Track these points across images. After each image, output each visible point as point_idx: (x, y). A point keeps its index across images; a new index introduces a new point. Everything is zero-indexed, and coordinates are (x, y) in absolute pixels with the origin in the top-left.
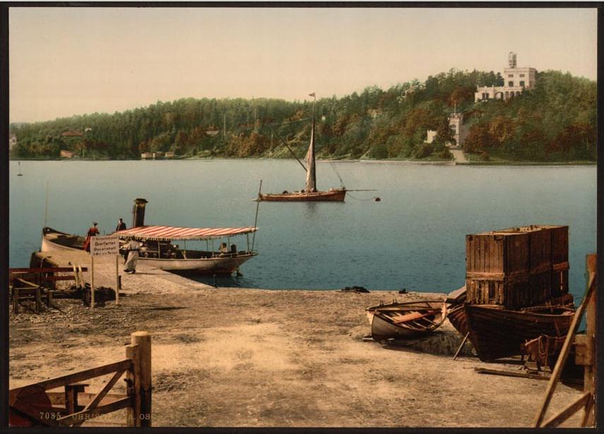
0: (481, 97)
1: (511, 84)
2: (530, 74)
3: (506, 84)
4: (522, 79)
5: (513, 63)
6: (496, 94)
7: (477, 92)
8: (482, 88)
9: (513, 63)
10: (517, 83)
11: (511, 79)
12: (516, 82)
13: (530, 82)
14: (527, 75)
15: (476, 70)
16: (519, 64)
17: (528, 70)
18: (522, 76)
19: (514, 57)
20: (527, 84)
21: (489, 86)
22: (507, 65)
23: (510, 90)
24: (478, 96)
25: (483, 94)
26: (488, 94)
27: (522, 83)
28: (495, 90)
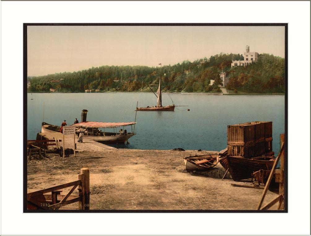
1: (247, 59)
3: (245, 59)
4: (252, 57)
5: (248, 50)
6: (240, 64)
7: (232, 63)
9: (248, 50)
10: (249, 59)
11: (247, 57)
12: (249, 59)
13: (256, 59)
14: (254, 55)
16: (251, 51)
17: (254, 53)
18: (252, 56)
19: (249, 47)
20: (254, 59)
22: (245, 51)
23: (246, 62)
24: (233, 65)
25: (235, 64)
26: (237, 64)
27: (252, 59)
28: (240, 62)
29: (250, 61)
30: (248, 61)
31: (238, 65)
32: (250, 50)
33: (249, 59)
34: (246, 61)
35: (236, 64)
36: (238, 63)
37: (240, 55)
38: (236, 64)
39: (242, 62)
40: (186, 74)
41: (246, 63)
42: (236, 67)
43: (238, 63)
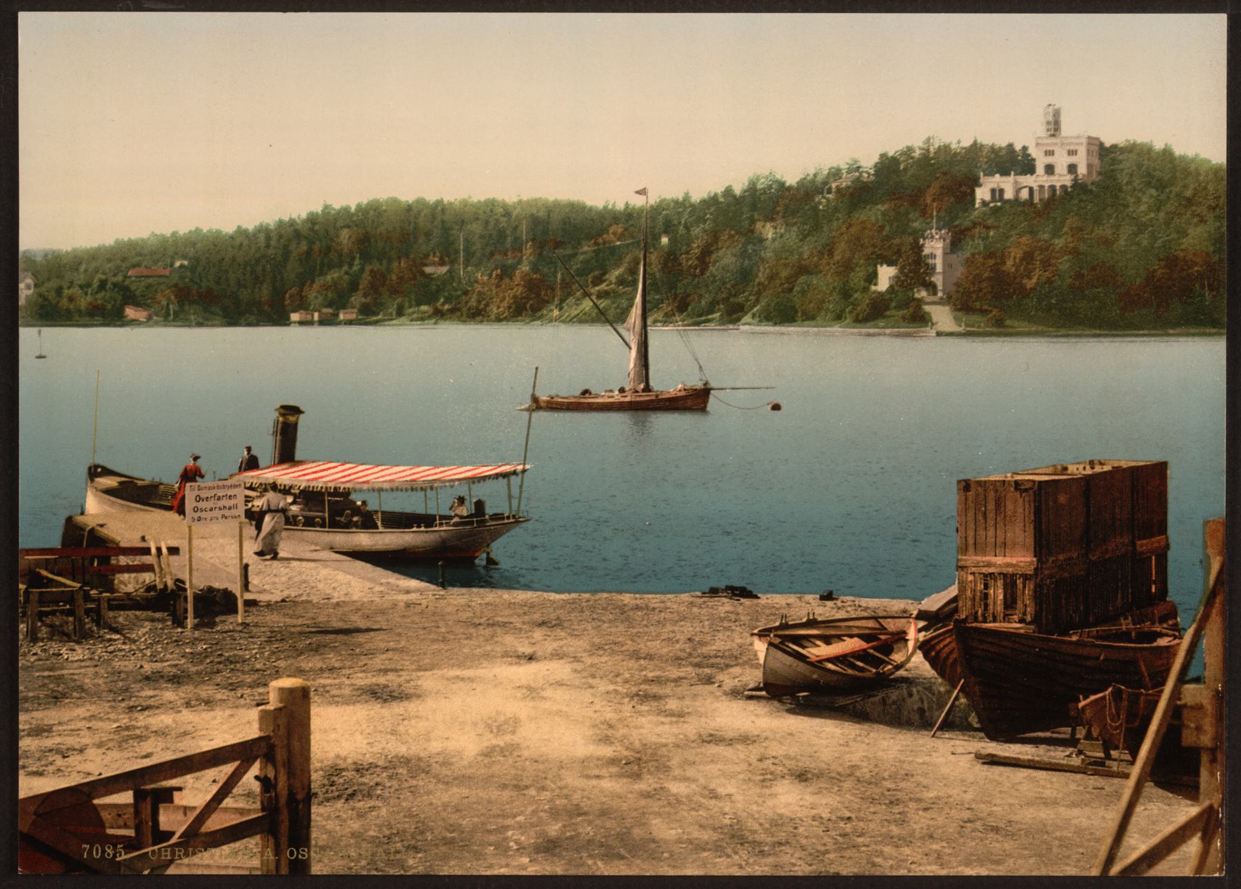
1: (1050, 169)
3: (1040, 169)
4: (1073, 160)
5: (1055, 127)
6: (1018, 191)
7: (980, 186)
8: (990, 179)
9: (1055, 127)
11: (1049, 160)
12: (1060, 167)
13: (1089, 166)
14: (1082, 151)
16: (1066, 130)
17: (1084, 141)
18: (1072, 153)
19: (1057, 114)
20: (1082, 170)
21: (1005, 173)
22: (1041, 131)
23: (1046, 181)
24: (982, 194)
25: (993, 191)
26: (1002, 191)
27: (1072, 168)
28: (1016, 182)
29: (1062, 179)
30: (1052, 178)
31: (1009, 195)
32: (1064, 120)
34: (1045, 178)
35: (997, 193)
36: (1008, 185)
38: (997, 193)
39: (1028, 180)
40: (761, 240)
41: (1047, 185)
42: (1001, 207)
43: (1008, 185)
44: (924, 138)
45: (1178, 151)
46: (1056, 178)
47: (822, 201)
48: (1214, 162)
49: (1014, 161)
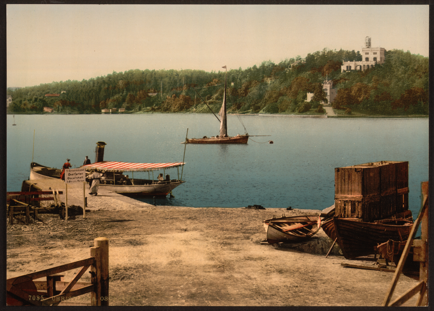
0: (345, 69)
1: (367, 59)
2: (381, 53)
3: (364, 59)
4: (375, 56)
5: (369, 44)
6: (356, 67)
7: (343, 65)
8: (346, 63)
9: (369, 44)
10: (371, 59)
11: (367, 56)
12: (371, 58)
13: (381, 58)
14: (378, 53)
15: (342, 50)
16: (373, 45)
17: (379, 49)
18: (375, 53)
19: (370, 40)
20: (378, 59)
22: (364, 46)
23: (366, 63)
24: (343, 68)
25: (347, 67)
26: (350, 67)
27: (375, 59)
28: (355, 64)
29: (372, 63)
30: (368, 62)
31: (353, 68)
33: (371, 59)
34: (366, 62)
35: (349, 68)
36: (352, 65)
37: (356, 52)
38: (349, 68)
39: (359, 63)
40: (266, 84)
42: (350, 72)
44: (323, 48)
45: (412, 53)
46: (369, 62)
47: (287, 70)
48: (425, 57)
49: (355, 56)
